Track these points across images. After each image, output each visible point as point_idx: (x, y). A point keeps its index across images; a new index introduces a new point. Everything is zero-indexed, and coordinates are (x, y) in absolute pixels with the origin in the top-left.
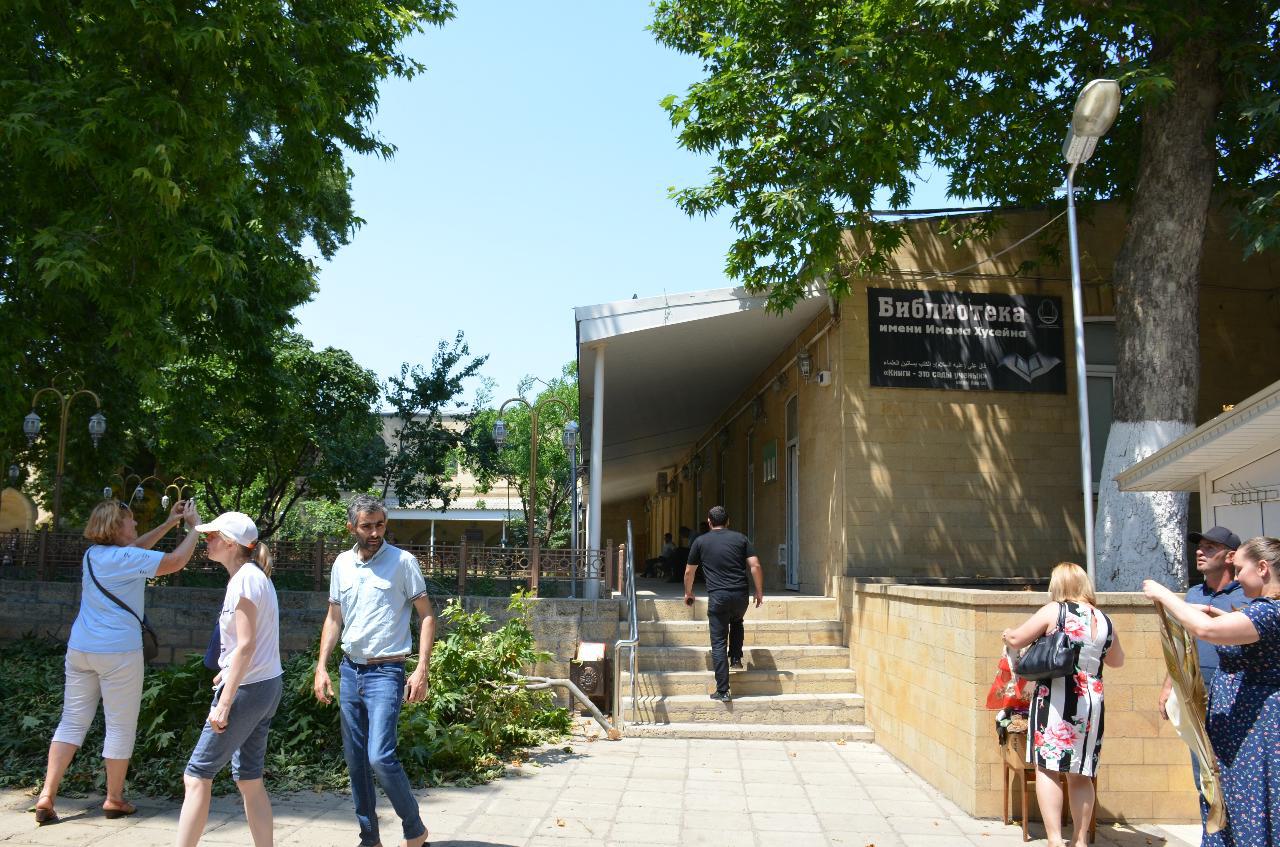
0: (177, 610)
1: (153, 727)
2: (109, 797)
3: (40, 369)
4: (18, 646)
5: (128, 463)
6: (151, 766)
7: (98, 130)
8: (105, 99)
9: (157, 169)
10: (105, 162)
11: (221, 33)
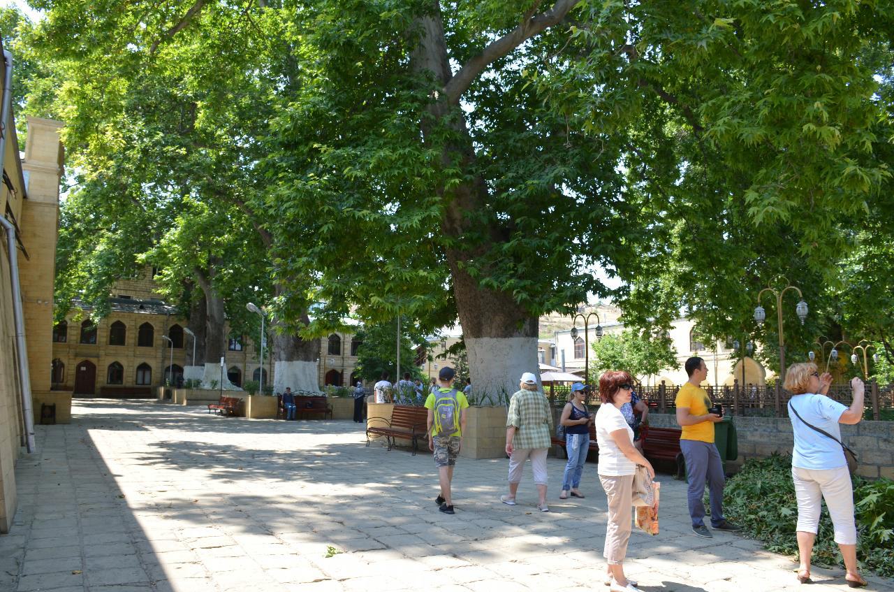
0: (879, 438)
1: (875, 524)
2: (848, 571)
3: (756, 278)
4: (769, 461)
5: (824, 333)
6: (877, 553)
7: (770, 113)
8: (770, 91)
9: (818, 120)
10: (778, 133)
11: (837, 14)
